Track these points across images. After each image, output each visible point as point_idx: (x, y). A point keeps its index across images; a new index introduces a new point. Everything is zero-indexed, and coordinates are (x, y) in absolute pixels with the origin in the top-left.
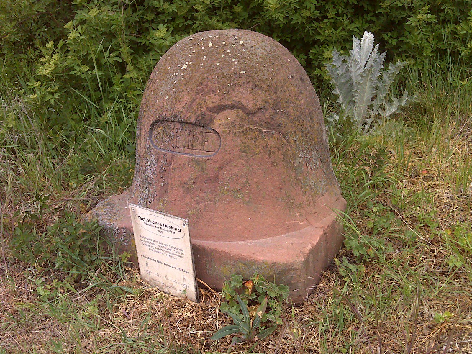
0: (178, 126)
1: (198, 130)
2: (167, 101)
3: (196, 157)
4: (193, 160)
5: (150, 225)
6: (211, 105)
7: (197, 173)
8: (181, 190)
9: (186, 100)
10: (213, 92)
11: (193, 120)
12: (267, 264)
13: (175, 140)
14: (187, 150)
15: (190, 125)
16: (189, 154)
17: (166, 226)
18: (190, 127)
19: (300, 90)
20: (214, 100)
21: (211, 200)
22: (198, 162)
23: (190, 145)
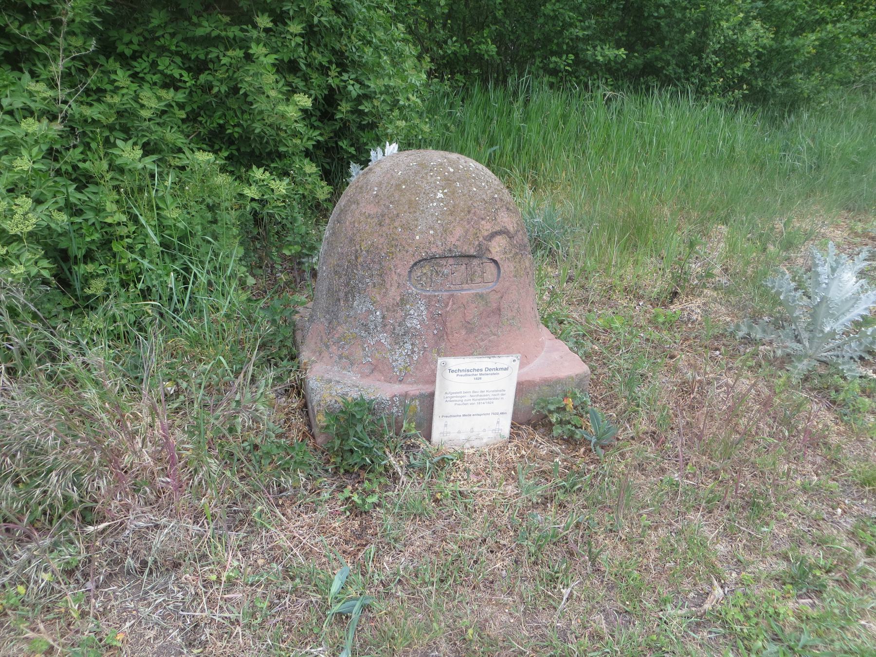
0: (451, 261)
1: (475, 262)
2: (433, 236)
3: (479, 291)
4: (477, 295)
5: (466, 375)
6: (486, 233)
7: (482, 309)
8: (463, 332)
9: (459, 232)
10: (482, 219)
11: (472, 252)
12: (572, 378)
13: (450, 278)
14: (465, 286)
15: (466, 259)
16: (469, 290)
17: (490, 370)
18: (466, 260)
19: (13, 120)
20: (487, 227)
21: (494, 335)
22: (481, 296)
23: (470, 279)
